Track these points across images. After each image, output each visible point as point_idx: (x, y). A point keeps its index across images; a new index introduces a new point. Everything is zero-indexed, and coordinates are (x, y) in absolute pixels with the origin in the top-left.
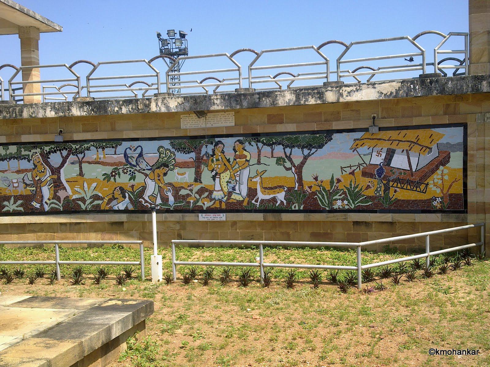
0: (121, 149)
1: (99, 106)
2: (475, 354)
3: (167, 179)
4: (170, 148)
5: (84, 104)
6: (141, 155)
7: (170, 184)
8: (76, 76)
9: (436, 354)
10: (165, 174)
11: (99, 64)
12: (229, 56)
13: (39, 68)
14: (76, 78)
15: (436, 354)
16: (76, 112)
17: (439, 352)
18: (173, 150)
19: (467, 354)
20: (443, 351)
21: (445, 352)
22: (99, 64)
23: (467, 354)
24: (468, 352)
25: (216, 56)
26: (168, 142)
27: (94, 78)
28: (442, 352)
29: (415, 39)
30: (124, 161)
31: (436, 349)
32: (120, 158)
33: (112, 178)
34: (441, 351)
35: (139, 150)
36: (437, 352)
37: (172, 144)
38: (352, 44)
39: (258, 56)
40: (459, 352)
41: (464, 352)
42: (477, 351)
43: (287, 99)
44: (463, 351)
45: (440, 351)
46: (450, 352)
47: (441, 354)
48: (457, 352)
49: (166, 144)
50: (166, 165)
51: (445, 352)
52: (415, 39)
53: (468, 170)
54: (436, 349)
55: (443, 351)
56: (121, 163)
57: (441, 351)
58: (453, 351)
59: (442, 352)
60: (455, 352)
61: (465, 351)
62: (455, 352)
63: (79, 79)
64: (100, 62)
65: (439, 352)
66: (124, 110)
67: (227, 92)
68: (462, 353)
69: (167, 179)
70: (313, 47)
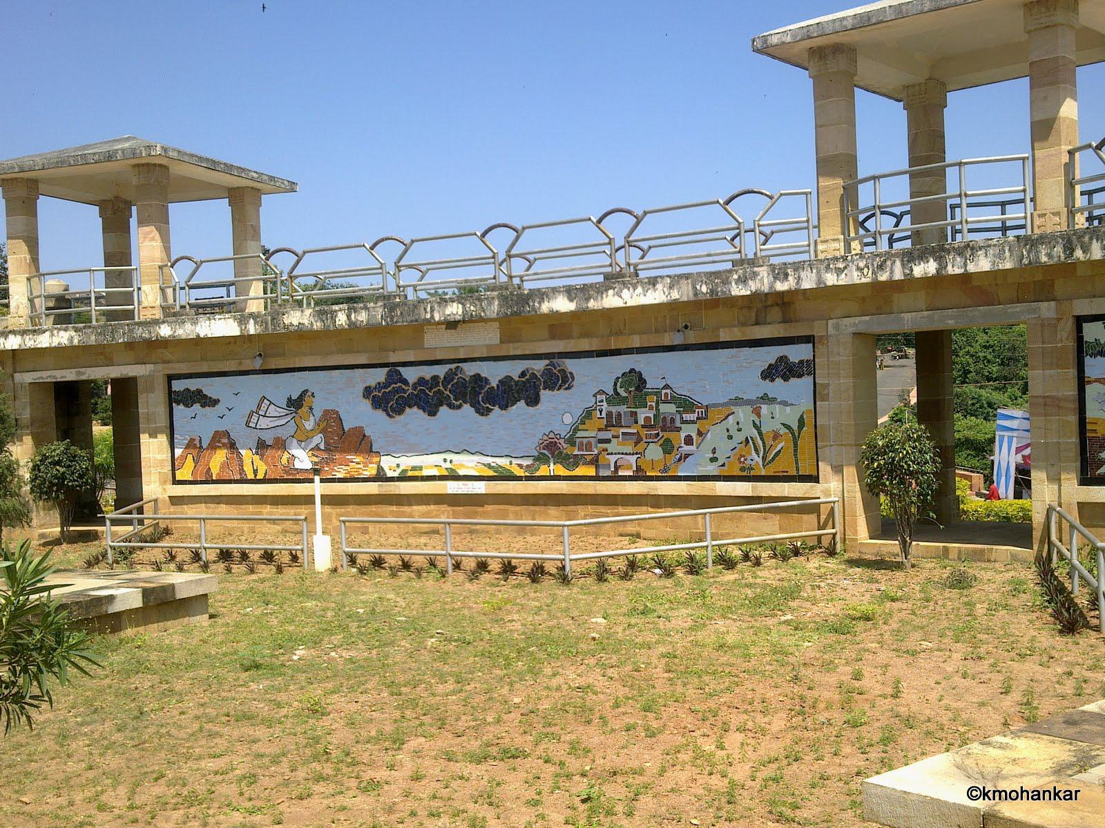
2: (1071, 799)
8: (608, 237)
9: (984, 799)
11: (413, 241)
12: (595, 221)
13: (1037, 169)
14: (607, 240)
15: (984, 799)
17: (990, 795)
20: (998, 791)
21: (1003, 794)
22: (413, 241)
24: (1056, 794)
25: (355, 247)
27: (299, 274)
28: (997, 794)
29: (727, 202)
31: (984, 788)
34: (994, 792)
38: (645, 213)
39: (519, 233)
40: (1036, 793)
42: (1076, 792)
43: (360, 318)
44: (1044, 792)
46: (1014, 795)
48: (1030, 795)
51: (1003, 794)
52: (727, 202)
54: (984, 788)
55: (1000, 792)
57: (994, 792)
58: (1022, 792)
59: (997, 794)
63: (612, 241)
64: (414, 238)
65: (990, 795)
68: (1041, 798)
70: (475, 234)
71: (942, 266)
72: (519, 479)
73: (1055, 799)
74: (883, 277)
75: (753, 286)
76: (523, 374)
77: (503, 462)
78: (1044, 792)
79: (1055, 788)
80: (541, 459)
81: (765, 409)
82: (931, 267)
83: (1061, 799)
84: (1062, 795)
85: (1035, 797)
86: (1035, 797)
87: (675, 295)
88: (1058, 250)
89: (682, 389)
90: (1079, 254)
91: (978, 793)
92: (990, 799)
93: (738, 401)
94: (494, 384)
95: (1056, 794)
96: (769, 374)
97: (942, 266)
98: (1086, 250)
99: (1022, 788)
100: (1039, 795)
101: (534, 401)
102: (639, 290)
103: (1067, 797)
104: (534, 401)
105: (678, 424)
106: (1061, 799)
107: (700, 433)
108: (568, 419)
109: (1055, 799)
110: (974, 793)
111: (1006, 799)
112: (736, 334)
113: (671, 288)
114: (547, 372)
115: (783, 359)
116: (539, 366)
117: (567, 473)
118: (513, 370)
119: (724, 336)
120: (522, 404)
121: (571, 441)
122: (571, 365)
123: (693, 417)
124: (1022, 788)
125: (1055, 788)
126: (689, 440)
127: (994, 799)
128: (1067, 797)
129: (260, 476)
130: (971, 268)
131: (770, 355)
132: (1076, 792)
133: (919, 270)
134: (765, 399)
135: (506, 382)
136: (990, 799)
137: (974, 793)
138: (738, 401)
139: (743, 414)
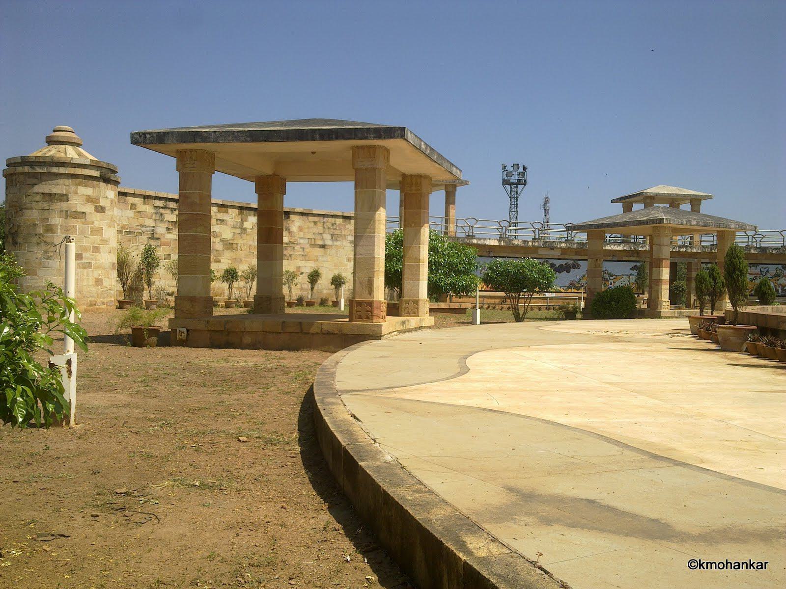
0: (759, 268)
1: (764, 250)
3: (779, 282)
4: (782, 268)
5: (756, 248)
6: (767, 271)
7: (780, 284)
9: (700, 569)
10: (778, 280)
15: (700, 569)
16: (753, 251)
17: (705, 565)
18: (782, 269)
19: (749, 567)
20: (710, 563)
21: (714, 565)
23: (749, 567)
24: (751, 565)
26: (781, 266)
28: (709, 565)
30: (760, 273)
31: (700, 560)
32: (758, 271)
33: (754, 281)
34: (707, 563)
35: (767, 269)
36: (701, 565)
37: (783, 268)
41: (745, 565)
42: (766, 563)
44: (743, 563)
45: (705, 563)
46: (721, 566)
47: (707, 569)
48: (733, 565)
49: (780, 267)
50: (779, 276)
51: (714, 565)
53: (352, 281)
54: (700, 560)
55: (711, 564)
56: (758, 274)
57: (707, 563)
58: (727, 563)
59: (709, 565)
60: (729, 564)
61: (746, 563)
62: (729, 564)
65: (705, 565)
66: (774, 252)
67: (363, 124)
69: (779, 282)
71: (686, 250)
72: (563, 292)
73: (750, 568)
74: (674, 250)
75: (644, 249)
76: (566, 264)
77: (559, 288)
78: (743, 563)
79: (750, 560)
80: (569, 287)
81: (631, 277)
82: (684, 250)
83: (754, 569)
84: (755, 565)
85: (736, 567)
86: (736, 567)
87: (625, 248)
88: (709, 249)
89: (610, 271)
90: (713, 251)
91: (696, 564)
92: (704, 569)
93: (624, 275)
94: (557, 266)
95: (751, 565)
96: (632, 269)
97: (686, 250)
98: (715, 250)
99: (727, 560)
100: (762, 565)
101: (568, 271)
102: (616, 246)
103: (759, 567)
104: (568, 271)
105: (608, 279)
106: (754, 569)
107: (614, 282)
108: (578, 277)
109: (750, 568)
110: (693, 564)
111: (716, 568)
112: (627, 259)
113: (624, 246)
114: (573, 264)
115: (636, 266)
116: (571, 262)
117: (577, 291)
118: (563, 262)
119: (624, 259)
120: (565, 272)
121: (579, 283)
122: (580, 262)
123: (613, 278)
124: (727, 560)
125: (750, 560)
126: (611, 284)
127: (707, 569)
128: (759, 567)
129: (483, 289)
130: (692, 251)
131: (634, 264)
132: (766, 563)
133: (681, 250)
134: (631, 275)
135: (561, 266)
136: (704, 569)
137: (693, 564)
138: (624, 275)
139: (625, 278)
